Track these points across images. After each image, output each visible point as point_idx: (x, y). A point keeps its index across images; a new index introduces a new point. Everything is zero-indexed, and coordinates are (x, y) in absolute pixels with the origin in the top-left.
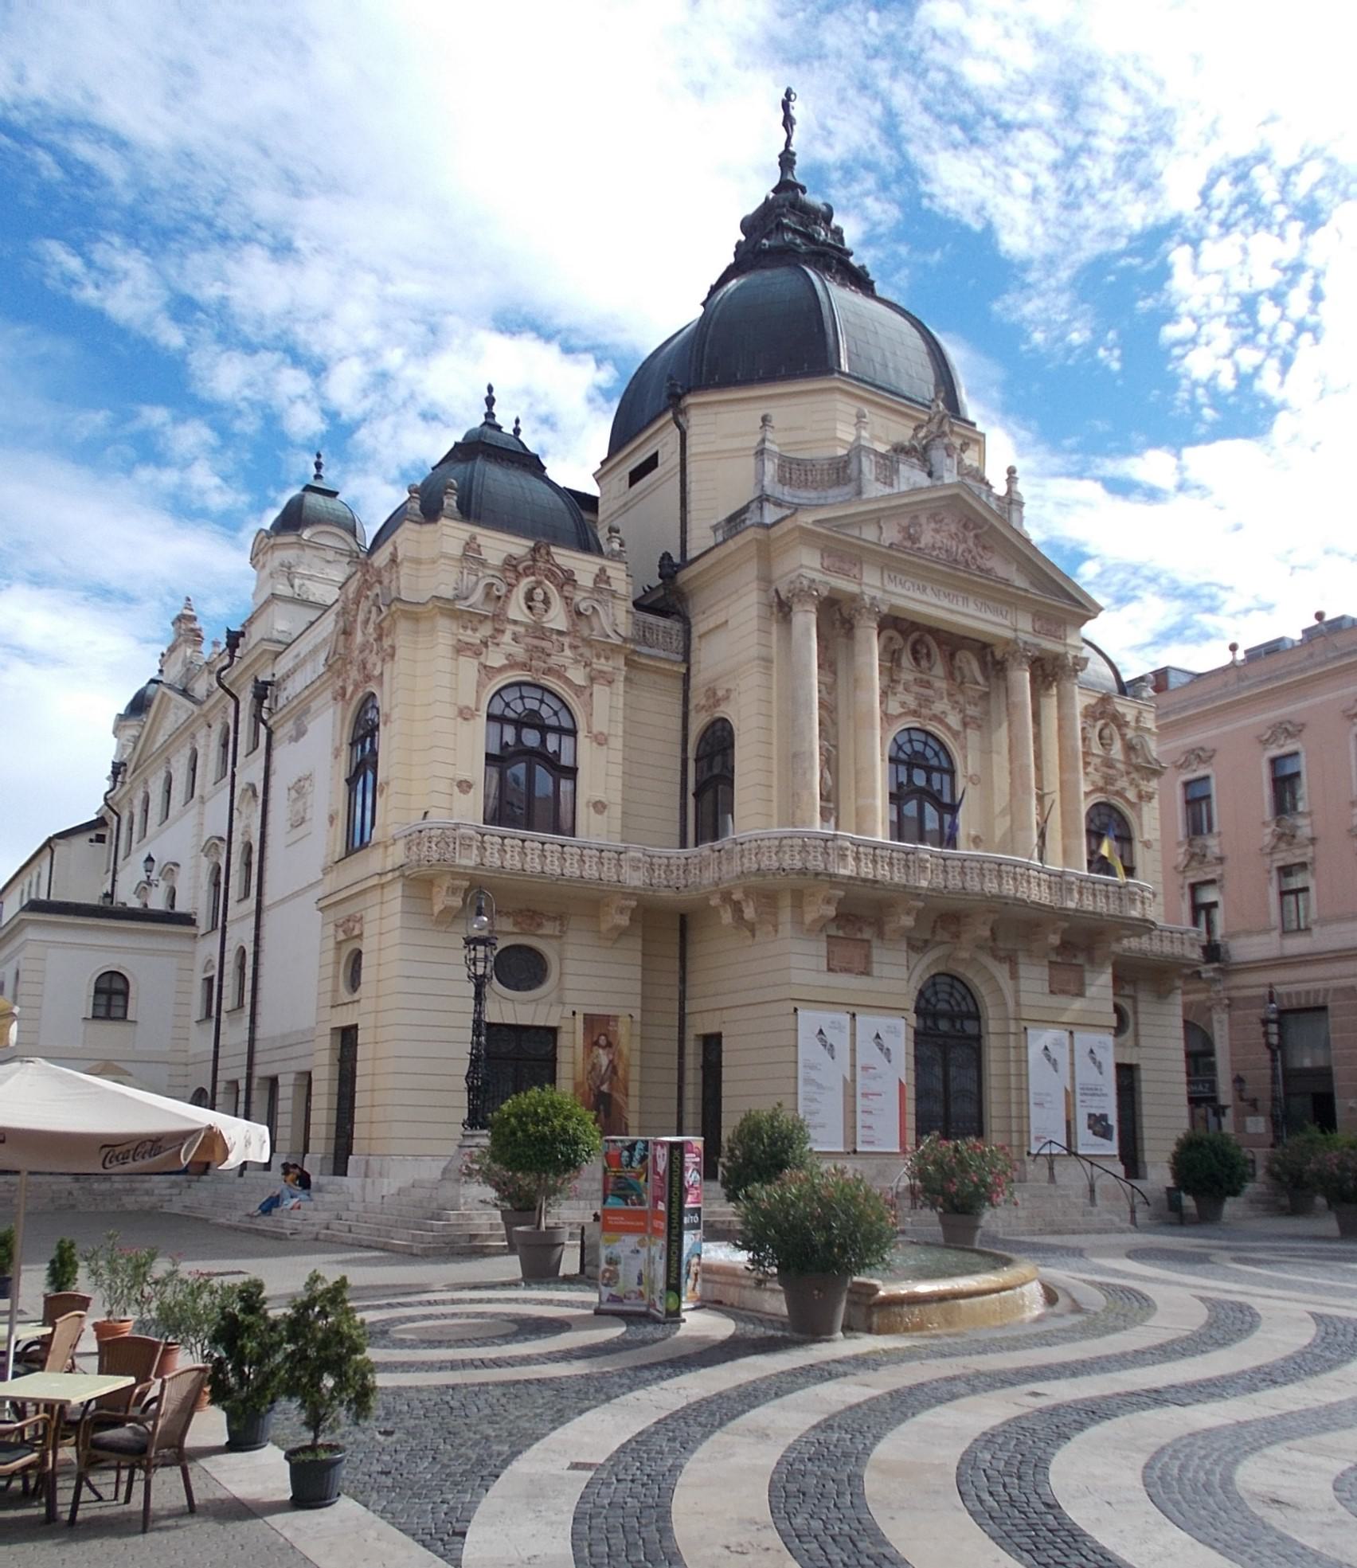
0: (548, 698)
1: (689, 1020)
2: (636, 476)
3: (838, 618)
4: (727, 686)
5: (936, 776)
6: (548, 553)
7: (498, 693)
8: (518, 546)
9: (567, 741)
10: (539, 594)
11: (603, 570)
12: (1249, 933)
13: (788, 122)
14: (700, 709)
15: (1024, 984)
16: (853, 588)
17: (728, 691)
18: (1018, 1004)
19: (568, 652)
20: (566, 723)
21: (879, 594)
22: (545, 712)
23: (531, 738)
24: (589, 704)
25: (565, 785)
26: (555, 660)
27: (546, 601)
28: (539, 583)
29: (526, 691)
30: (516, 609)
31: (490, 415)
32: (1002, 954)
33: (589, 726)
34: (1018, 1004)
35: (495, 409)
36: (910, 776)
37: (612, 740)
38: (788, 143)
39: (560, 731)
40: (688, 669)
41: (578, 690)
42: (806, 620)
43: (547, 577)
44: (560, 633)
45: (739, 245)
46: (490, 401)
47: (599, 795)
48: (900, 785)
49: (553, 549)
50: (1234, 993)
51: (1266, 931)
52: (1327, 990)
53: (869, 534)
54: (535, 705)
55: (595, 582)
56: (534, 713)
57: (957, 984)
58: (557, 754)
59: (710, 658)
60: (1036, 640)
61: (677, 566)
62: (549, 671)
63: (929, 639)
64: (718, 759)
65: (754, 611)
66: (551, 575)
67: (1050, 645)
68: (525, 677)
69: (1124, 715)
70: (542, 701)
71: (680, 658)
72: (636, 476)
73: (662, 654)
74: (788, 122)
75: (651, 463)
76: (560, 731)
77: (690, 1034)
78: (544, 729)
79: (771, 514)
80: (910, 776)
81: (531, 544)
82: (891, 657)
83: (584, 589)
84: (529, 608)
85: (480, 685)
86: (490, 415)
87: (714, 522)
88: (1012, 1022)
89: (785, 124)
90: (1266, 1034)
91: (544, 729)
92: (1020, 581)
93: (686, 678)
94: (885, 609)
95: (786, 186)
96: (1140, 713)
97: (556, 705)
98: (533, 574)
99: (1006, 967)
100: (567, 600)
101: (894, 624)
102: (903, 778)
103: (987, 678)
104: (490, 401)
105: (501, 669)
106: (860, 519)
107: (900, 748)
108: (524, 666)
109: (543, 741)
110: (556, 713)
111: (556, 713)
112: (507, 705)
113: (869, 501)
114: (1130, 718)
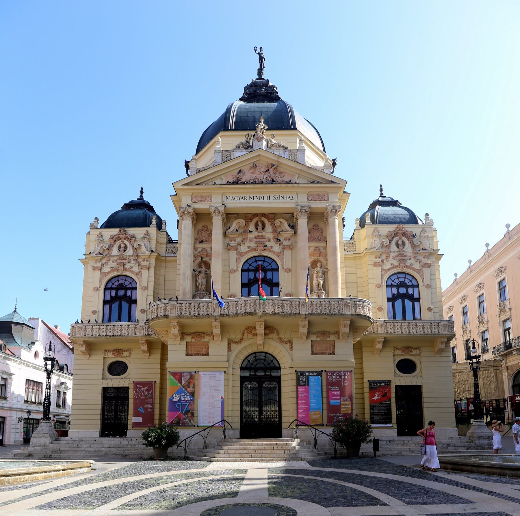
0: (407, 276)
8: (392, 228)
10: (400, 242)
11: (147, 232)
19: (133, 262)
20: (414, 283)
22: (407, 281)
23: (403, 291)
25: (417, 304)
26: (409, 262)
29: (399, 275)
30: (115, 252)
35: (143, 195)
37: (374, 286)
41: (418, 271)
43: (125, 239)
44: (129, 256)
46: (142, 192)
49: (127, 229)
54: (402, 279)
56: (121, 285)
57: (267, 355)
58: (412, 295)
62: (406, 267)
63: (263, 219)
66: (126, 238)
70: (398, 278)
84: (398, 247)
85: (101, 280)
97: (410, 278)
98: (398, 236)
99: (288, 346)
100: (411, 242)
101: (229, 216)
105: (389, 270)
108: (397, 267)
109: (407, 291)
110: (411, 281)
112: (393, 281)
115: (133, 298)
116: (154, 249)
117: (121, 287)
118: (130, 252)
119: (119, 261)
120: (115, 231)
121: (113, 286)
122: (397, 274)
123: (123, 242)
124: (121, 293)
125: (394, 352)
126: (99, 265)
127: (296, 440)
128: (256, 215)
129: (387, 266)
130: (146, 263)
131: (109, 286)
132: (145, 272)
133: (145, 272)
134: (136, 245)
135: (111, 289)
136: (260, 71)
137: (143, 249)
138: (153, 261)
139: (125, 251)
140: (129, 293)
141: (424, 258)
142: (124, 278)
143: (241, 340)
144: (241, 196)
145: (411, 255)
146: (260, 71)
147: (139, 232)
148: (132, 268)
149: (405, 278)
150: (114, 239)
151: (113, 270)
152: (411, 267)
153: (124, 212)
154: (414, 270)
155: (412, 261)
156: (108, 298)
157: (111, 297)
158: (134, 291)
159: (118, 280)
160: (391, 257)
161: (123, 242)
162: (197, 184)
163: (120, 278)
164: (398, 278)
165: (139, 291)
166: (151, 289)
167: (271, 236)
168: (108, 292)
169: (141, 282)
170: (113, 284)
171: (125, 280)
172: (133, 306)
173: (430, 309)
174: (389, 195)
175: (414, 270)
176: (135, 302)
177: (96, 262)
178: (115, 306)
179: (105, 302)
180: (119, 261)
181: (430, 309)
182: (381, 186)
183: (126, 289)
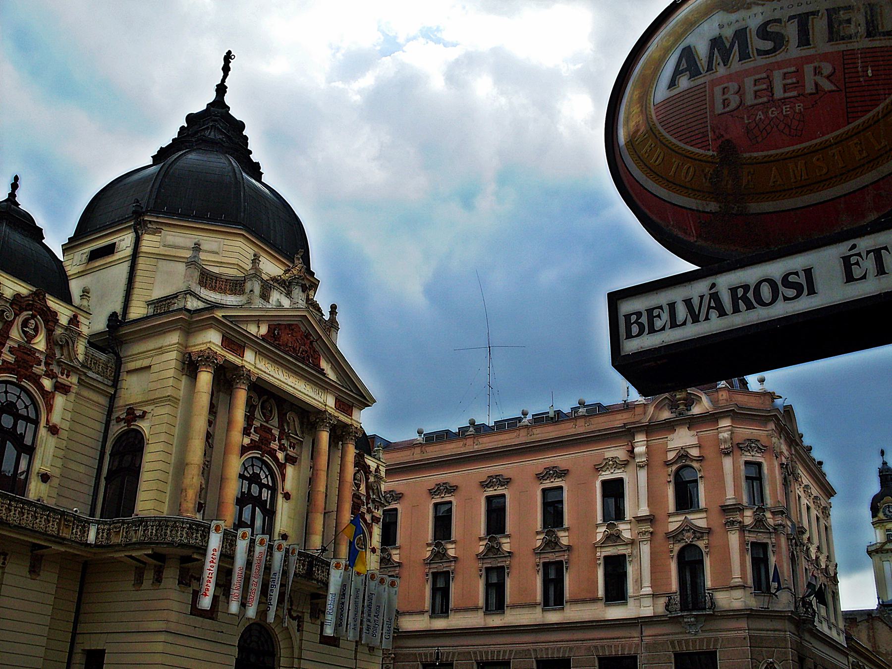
0: (23, 396)
1: (80, 639)
2: (94, 255)
3: (226, 378)
4: (145, 409)
5: (21, 424)
6: (44, 299)
7: (252, 458)
8: (24, 289)
9: (31, 427)
11: (75, 316)
12: (411, 613)
13: (226, 69)
14: (119, 420)
15: (306, 636)
16: (237, 361)
17: (145, 413)
18: (300, 649)
20: (32, 415)
21: (252, 368)
22: (20, 405)
24: (50, 408)
27: (36, 330)
28: (33, 317)
31: (12, 195)
32: (295, 615)
34: (300, 649)
36: (249, 488)
38: (223, 80)
39: (27, 419)
40: (115, 392)
42: (205, 378)
45: (182, 128)
46: (15, 186)
47: (46, 469)
48: (243, 493)
50: (399, 651)
51: (422, 613)
52: (454, 654)
53: (252, 329)
55: (69, 323)
58: (22, 436)
59: (133, 389)
60: (336, 414)
61: (120, 321)
63: (272, 401)
64: (128, 458)
65: (173, 364)
67: (343, 418)
68: (13, 378)
69: (369, 466)
70: (19, 397)
71: (110, 383)
72: (94, 255)
73: (100, 378)
74: (226, 69)
75: (110, 250)
76: (27, 419)
77: (78, 649)
78: (17, 417)
79: (193, 304)
80: (249, 488)
81: (34, 289)
82: (250, 407)
83: (62, 326)
86: (12, 195)
87: (149, 299)
88: (296, 660)
89: (229, 69)
91: (17, 417)
92: (331, 375)
93: (112, 398)
94: (253, 379)
95: (219, 105)
96: (378, 467)
102: (245, 490)
103: (303, 433)
104: (15, 186)
106: (248, 319)
107: (246, 469)
109: (15, 425)
110: (26, 407)
111: (26, 407)
113: (255, 309)
114: (373, 469)
132: (59, 401)
136: (221, 89)
141: (62, 374)
149: (19, 397)
162: (231, 322)
167: (276, 432)
173: (45, 478)
181: (45, 478)
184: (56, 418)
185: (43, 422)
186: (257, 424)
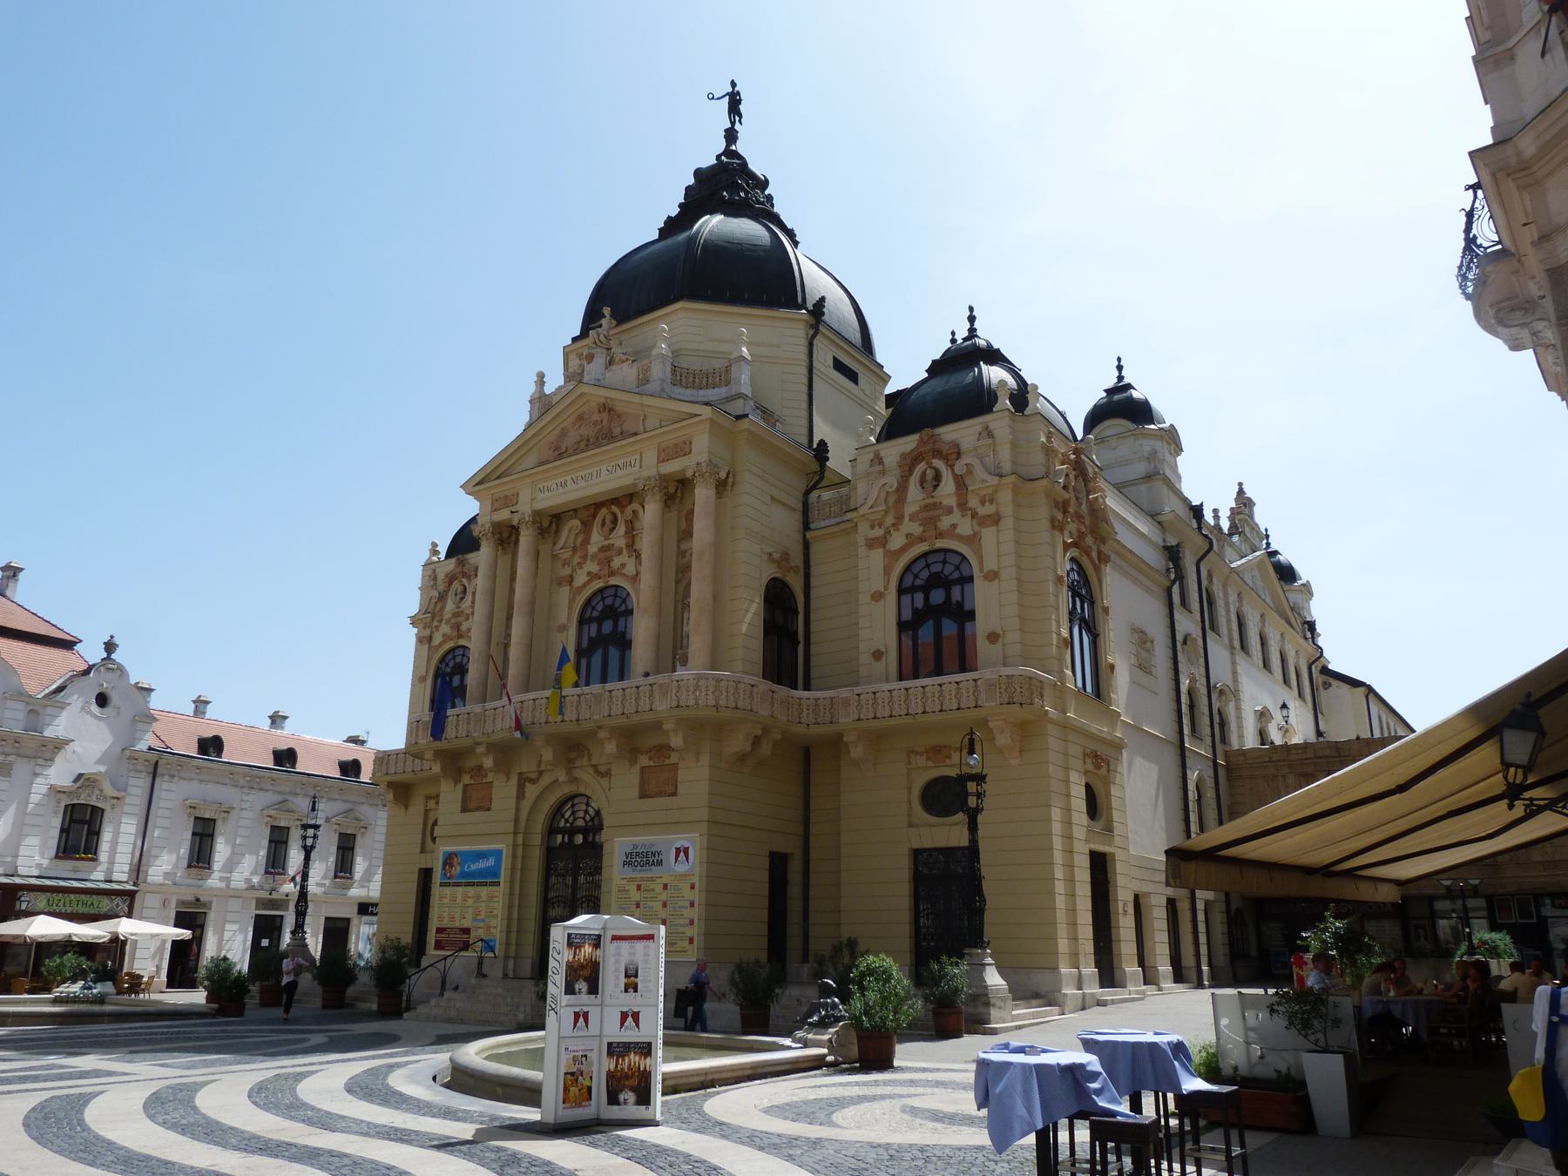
22: (948, 569)
26: (945, 522)
33: (981, 570)
35: (976, 325)
62: (940, 535)
66: (938, 453)
85: (887, 571)
90: (304, 838)
101: (550, 523)
108: (922, 539)
109: (948, 596)
115: (967, 607)
116: (1007, 467)
117: (937, 581)
118: (948, 486)
119: (924, 515)
120: (908, 443)
121: (919, 582)
122: (925, 555)
123: (930, 465)
124: (937, 596)
125: (909, 763)
126: (878, 532)
127: (160, 880)
128: (598, 506)
129: (897, 541)
130: (988, 509)
131: (908, 582)
132: (988, 534)
133: (988, 534)
134: (958, 470)
135: (913, 590)
136: (731, 136)
137: (979, 472)
138: (1005, 497)
139: (936, 487)
140: (956, 593)
142: (940, 557)
143: (541, 773)
144: (559, 480)
145: (951, 501)
146: (731, 136)
147: (962, 433)
148: (954, 526)
150: (910, 462)
151: (912, 540)
152: (951, 532)
153: (939, 384)
154: (961, 538)
155: (955, 517)
156: (907, 615)
157: (915, 611)
158: (966, 587)
159: (928, 566)
160: (907, 518)
161: (930, 465)
163: (931, 559)
164: (928, 566)
165: (978, 582)
166: (1008, 574)
168: (906, 599)
169: (981, 559)
170: (916, 576)
171: (944, 562)
172: (968, 625)
174: (988, 334)
175: (961, 538)
176: (971, 615)
177: (872, 527)
178: (926, 632)
179: (902, 626)
180: (924, 515)
182: (971, 309)
183: (947, 584)
184: (990, 564)
185: (976, 573)
186: (592, 549)
